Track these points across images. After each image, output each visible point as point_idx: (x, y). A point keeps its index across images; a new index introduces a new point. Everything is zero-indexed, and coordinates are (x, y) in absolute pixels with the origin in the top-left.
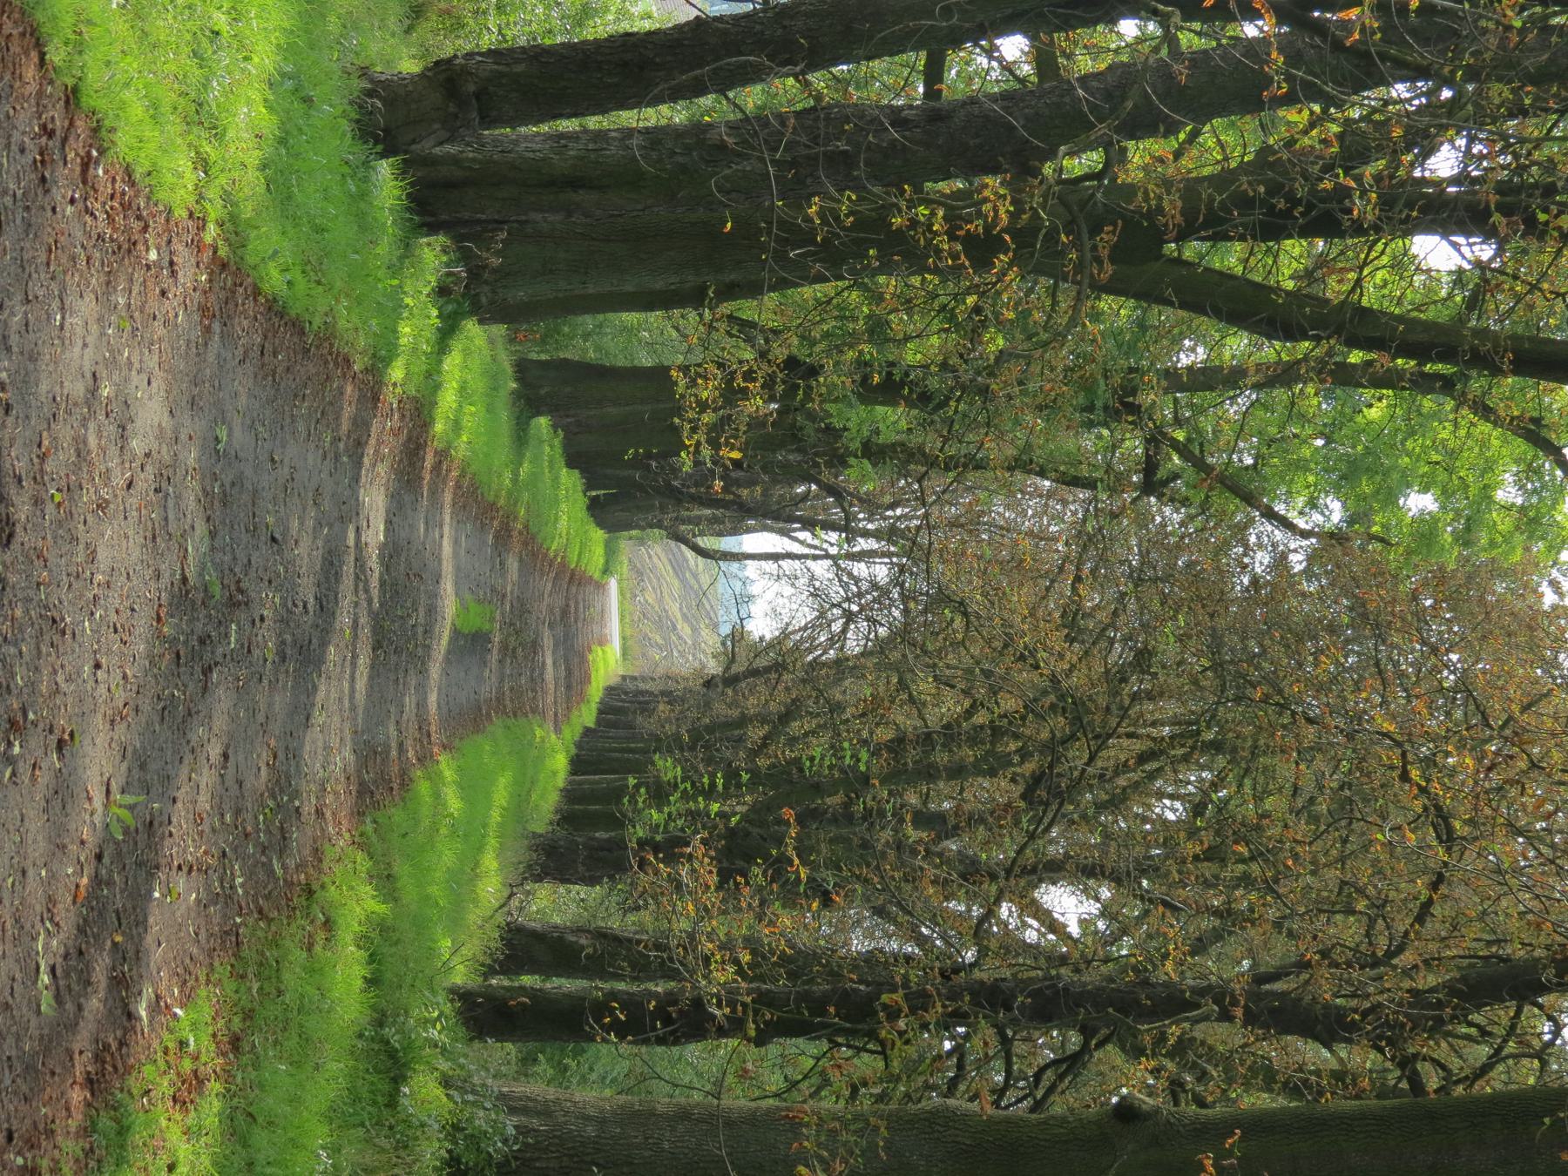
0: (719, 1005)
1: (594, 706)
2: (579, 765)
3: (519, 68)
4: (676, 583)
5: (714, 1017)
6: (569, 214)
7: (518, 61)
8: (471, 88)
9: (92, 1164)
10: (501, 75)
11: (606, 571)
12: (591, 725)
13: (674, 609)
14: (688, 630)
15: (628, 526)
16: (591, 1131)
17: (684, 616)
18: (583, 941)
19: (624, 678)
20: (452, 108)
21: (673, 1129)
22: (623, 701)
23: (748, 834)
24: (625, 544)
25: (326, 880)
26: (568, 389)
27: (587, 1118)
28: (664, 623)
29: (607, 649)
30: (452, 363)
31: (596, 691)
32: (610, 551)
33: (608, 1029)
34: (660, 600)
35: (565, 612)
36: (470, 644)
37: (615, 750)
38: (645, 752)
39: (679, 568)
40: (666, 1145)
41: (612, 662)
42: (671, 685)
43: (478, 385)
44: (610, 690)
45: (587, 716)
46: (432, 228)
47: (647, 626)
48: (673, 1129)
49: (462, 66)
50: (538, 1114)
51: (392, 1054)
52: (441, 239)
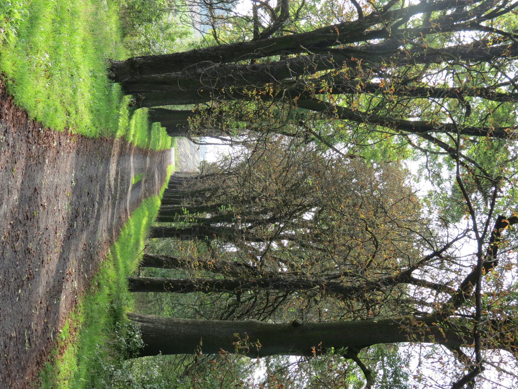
0: (197, 285)
1: (168, 182)
2: (163, 202)
3: (150, 61)
4: (189, 145)
5: (195, 287)
6: (162, 91)
7: (149, 59)
8: (138, 66)
9: (39, 385)
10: (145, 63)
11: (172, 146)
12: (167, 188)
13: (188, 152)
14: (192, 157)
15: (177, 136)
16: (164, 327)
17: (191, 154)
18: (163, 259)
19: (176, 172)
20: (132, 71)
21: (184, 327)
22: (175, 180)
23: (205, 228)
24: (176, 139)
25: (99, 273)
26: (162, 116)
27: (163, 324)
28: (186, 156)
29: (171, 165)
30: (133, 122)
31: (168, 178)
32: (172, 141)
33: (169, 290)
34: (185, 150)
35: (161, 162)
36: (138, 185)
37: (173, 197)
38: (180, 198)
39: (191, 145)
40: (182, 331)
41: (172, 168)
42: (187, 176)
43: (139, 126)
44: (172, 177)
45: (166, 186)
46: (127, 93)
47: (181, 158)
48: (184, 327)
49: (135, 61)
50: (151, 323)
51: (115, 311)
52: (131, 96)
